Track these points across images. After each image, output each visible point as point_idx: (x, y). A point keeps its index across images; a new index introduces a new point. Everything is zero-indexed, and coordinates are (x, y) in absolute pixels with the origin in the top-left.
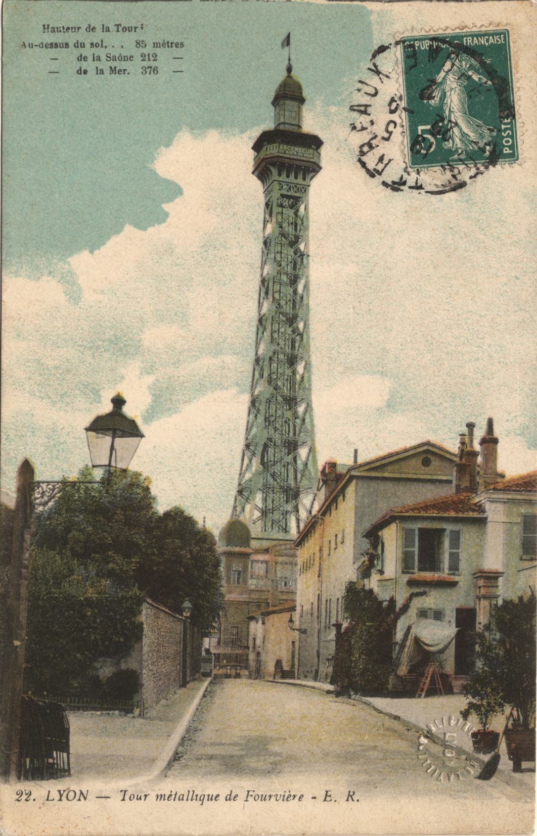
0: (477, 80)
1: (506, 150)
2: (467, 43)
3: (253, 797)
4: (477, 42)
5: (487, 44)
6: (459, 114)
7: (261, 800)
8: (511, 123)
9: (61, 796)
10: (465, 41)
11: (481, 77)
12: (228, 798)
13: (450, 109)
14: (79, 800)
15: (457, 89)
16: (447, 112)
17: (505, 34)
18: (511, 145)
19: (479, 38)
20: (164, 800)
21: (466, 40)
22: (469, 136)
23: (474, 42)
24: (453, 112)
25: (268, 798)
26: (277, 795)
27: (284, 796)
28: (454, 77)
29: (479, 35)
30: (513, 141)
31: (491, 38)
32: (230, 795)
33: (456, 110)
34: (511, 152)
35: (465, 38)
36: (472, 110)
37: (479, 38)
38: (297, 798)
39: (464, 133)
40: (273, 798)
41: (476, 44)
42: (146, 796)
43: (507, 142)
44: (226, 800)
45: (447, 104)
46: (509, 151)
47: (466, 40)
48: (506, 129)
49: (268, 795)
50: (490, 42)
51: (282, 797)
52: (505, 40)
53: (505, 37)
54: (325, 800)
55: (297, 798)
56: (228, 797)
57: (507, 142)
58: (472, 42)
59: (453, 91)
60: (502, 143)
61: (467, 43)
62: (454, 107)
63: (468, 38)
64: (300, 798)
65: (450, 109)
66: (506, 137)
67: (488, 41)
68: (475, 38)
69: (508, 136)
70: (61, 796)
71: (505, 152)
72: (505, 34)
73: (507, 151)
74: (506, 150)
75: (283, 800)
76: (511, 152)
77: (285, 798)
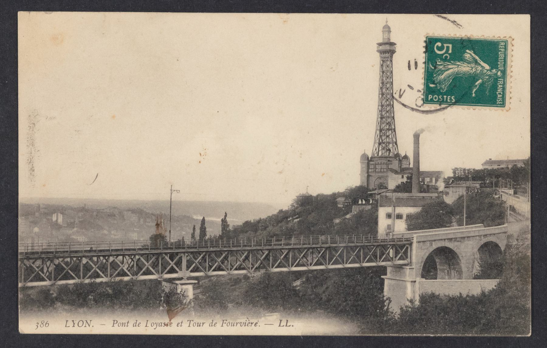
0: (476, 84)
1: (430, 97)
2: (500, 81)
3: (226, 324)
4: (499, 87)
5: (497, 93)
6: (457, 71)
7: (198, 326)
8: (447, 101)
9: (74, 324)
10: (501, 79)
11: (478, 87)
12: (134, 325)
13: (460, 65)
14: (85, 326)
15: (472, 71)
16: (458, 63)
17: (503, 105)
18: (434, 101)
19: (501, 89)
20: (124, 326)
21: (502, 81)
22: (441, 75)
23: (500, 85)
24: (458, 67)
25: (201, 325)
26: (241, 323)
27: (246, 323)
28: (480, 70)
29: (504, 89)
30: (436, 101)
31: (501, 96)
32: (136, 323)
33: (459, 69)
34: (429, 100)
35: (502, 80)
36: (457, 79)
37: (501, 89)
38: (254, 324)
39: (445, 72)
40: (239, 325)
41: (498, 86)
42: (203, 323)
43: (436, 98)
44: (134, 326)
45: (463, 64)
46: (429, 98)
47: (502, 81)
48: (443, 98)
49: (202, 323)
50: (499, 95)
51: (244, 324)
52: (499, 104)
53: (501, 104)
54: (280, 326)
55: (254, 324)
56: (135, 324)
57: (436, 98)
58: (500, 84)
59: (471, 69)
60: (434, 95)
61: (500, 81)
62: (461, 68)
63: (502, 82)
64: (255, 324)
65: (460, 65)
66: (439, 97)
67: (500, 94)
68: (502, 86)
69: (439, 99)
70: (74, 324)
71: (430, 96)
72: (503, 105)
73: (430, 97)
74: (430, 97)
75: (245, 326)
76: (429, 100)
77: (246, 324)
